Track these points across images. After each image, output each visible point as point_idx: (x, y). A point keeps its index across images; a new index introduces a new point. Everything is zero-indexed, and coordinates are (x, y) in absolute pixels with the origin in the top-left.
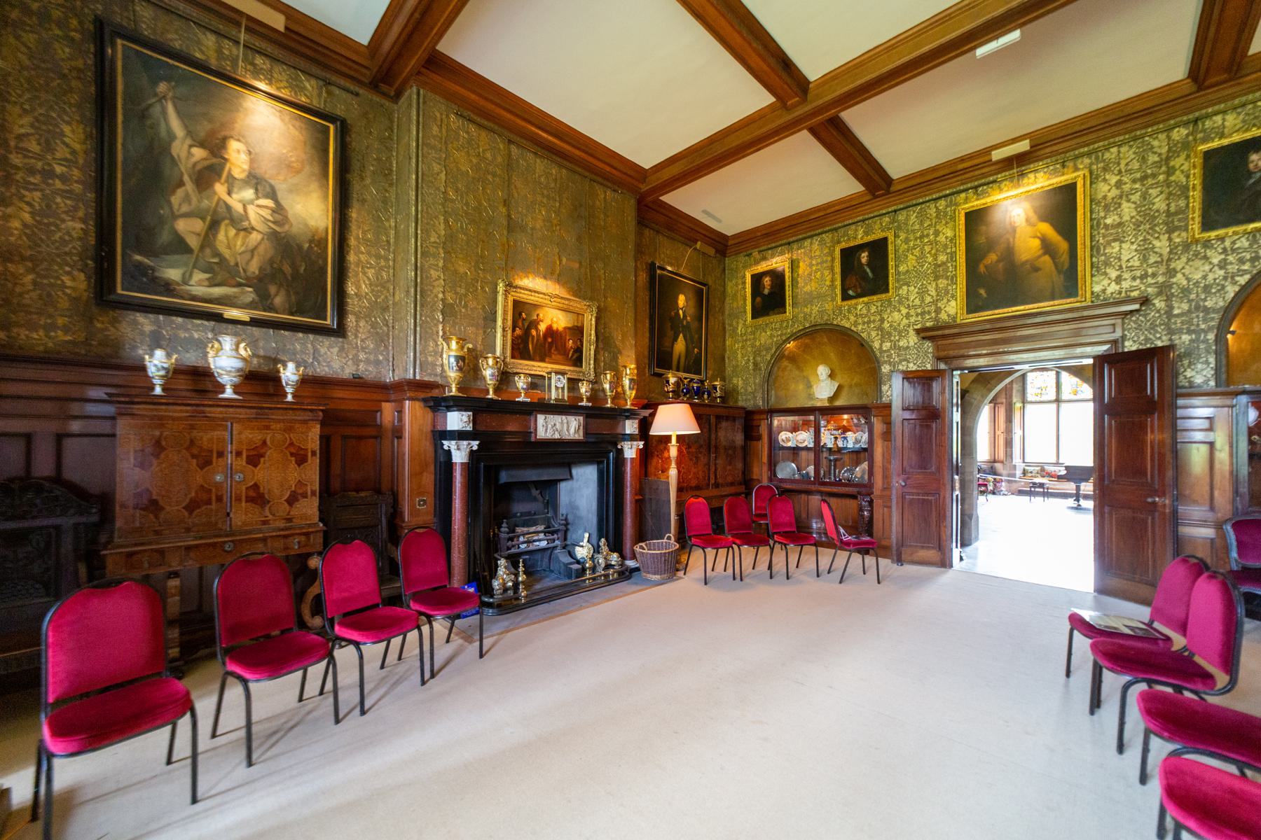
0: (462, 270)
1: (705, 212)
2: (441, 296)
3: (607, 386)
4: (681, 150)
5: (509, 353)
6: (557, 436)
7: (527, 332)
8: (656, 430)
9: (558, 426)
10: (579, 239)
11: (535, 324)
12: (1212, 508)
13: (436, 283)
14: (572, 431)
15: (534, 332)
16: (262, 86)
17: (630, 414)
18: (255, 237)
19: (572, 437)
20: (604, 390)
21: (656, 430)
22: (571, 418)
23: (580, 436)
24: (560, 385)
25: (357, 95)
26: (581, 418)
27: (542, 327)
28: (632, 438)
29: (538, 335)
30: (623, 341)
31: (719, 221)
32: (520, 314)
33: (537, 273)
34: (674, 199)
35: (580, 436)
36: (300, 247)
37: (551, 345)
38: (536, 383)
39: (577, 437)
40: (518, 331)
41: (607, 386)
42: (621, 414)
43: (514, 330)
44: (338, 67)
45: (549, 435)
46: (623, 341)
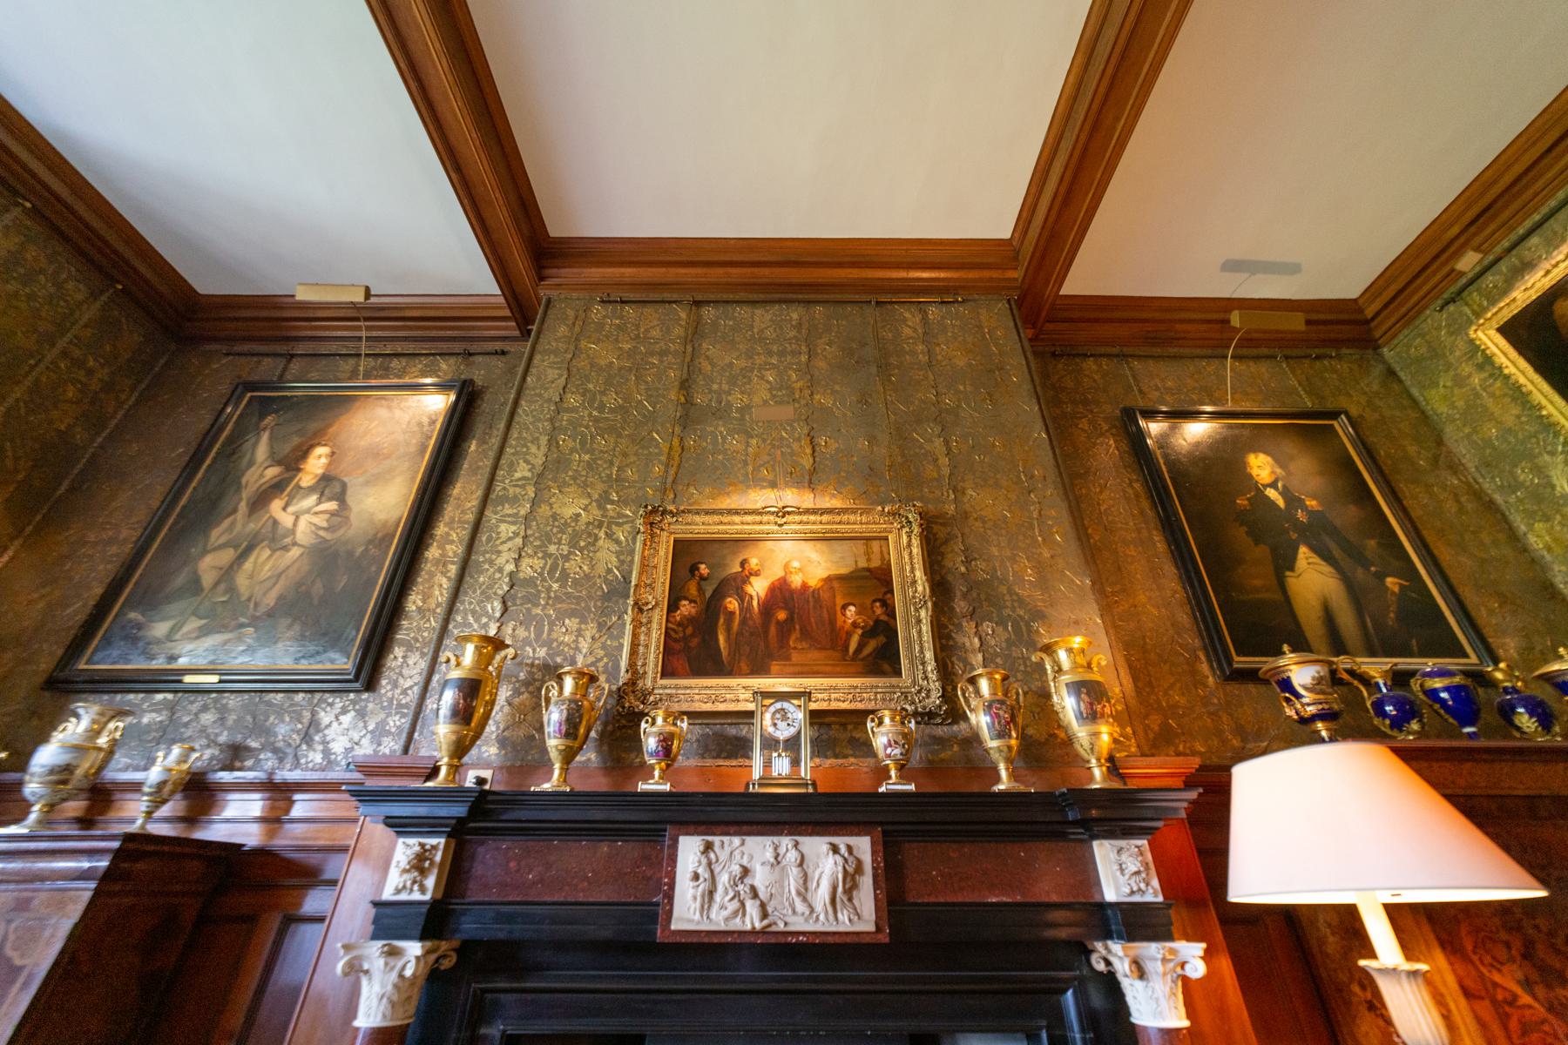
0: (568, 512)
1: (1232, 266)
2: (510, 567)
3: (981, 721)
4: (153, 243)
5: (652, 659)
6: (752, 920)
7: (712, 609)
8: (1259, 874)
9: (760, 878)
10: (864, 399)
11: (736, 585)
12: (707, 358)
13: (505, 547)
14: (822, 895)
15: (732, 604)
16: (428, 381)
17: (1118, 813)
18: (295, 552)
19: (823, 923)
20: (974, 739)
21: (1259, 874)
22: (817, 846)
23: (861, 917)
24: (784, 732)
25: (503, 353)
26: (863, 845)
27: (758, 588)
28: (1137, 923)
29: (746, 609)
30: (1043, 583)
31: (1293, 269)
32: (694, 569)
33: (756, 482)
34: (1096, 271)
35: (861, 917)
36: (350, 553)
37: (785, 629)
38: (727, 737)
39: (844, 923)
40: (686, 608)
41: (981, 721)
42: (1069, 814)
43: (673, 606)
44: (263, 334)
45: (720, 919)
46: (1043, 583)
